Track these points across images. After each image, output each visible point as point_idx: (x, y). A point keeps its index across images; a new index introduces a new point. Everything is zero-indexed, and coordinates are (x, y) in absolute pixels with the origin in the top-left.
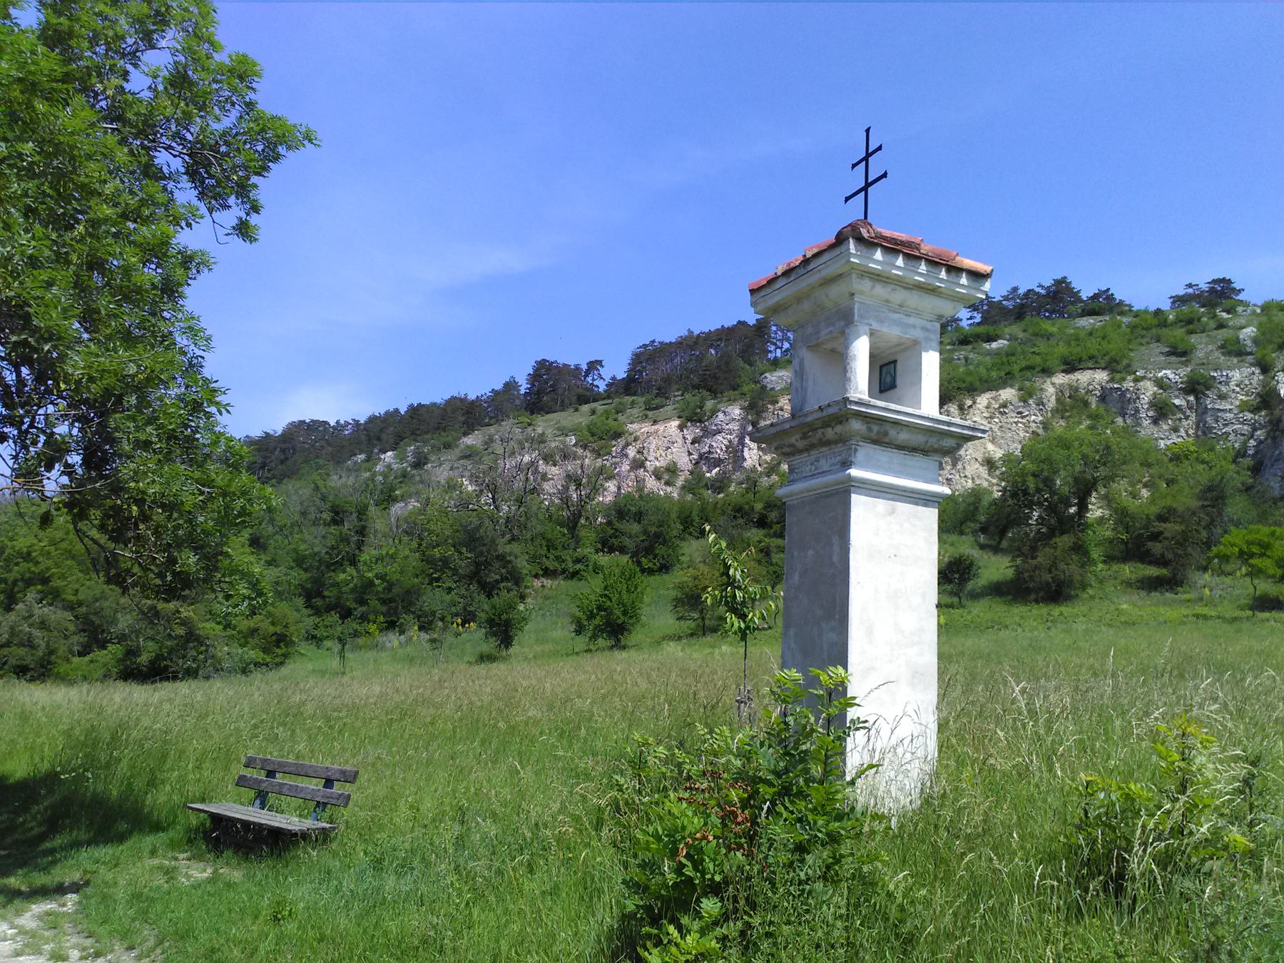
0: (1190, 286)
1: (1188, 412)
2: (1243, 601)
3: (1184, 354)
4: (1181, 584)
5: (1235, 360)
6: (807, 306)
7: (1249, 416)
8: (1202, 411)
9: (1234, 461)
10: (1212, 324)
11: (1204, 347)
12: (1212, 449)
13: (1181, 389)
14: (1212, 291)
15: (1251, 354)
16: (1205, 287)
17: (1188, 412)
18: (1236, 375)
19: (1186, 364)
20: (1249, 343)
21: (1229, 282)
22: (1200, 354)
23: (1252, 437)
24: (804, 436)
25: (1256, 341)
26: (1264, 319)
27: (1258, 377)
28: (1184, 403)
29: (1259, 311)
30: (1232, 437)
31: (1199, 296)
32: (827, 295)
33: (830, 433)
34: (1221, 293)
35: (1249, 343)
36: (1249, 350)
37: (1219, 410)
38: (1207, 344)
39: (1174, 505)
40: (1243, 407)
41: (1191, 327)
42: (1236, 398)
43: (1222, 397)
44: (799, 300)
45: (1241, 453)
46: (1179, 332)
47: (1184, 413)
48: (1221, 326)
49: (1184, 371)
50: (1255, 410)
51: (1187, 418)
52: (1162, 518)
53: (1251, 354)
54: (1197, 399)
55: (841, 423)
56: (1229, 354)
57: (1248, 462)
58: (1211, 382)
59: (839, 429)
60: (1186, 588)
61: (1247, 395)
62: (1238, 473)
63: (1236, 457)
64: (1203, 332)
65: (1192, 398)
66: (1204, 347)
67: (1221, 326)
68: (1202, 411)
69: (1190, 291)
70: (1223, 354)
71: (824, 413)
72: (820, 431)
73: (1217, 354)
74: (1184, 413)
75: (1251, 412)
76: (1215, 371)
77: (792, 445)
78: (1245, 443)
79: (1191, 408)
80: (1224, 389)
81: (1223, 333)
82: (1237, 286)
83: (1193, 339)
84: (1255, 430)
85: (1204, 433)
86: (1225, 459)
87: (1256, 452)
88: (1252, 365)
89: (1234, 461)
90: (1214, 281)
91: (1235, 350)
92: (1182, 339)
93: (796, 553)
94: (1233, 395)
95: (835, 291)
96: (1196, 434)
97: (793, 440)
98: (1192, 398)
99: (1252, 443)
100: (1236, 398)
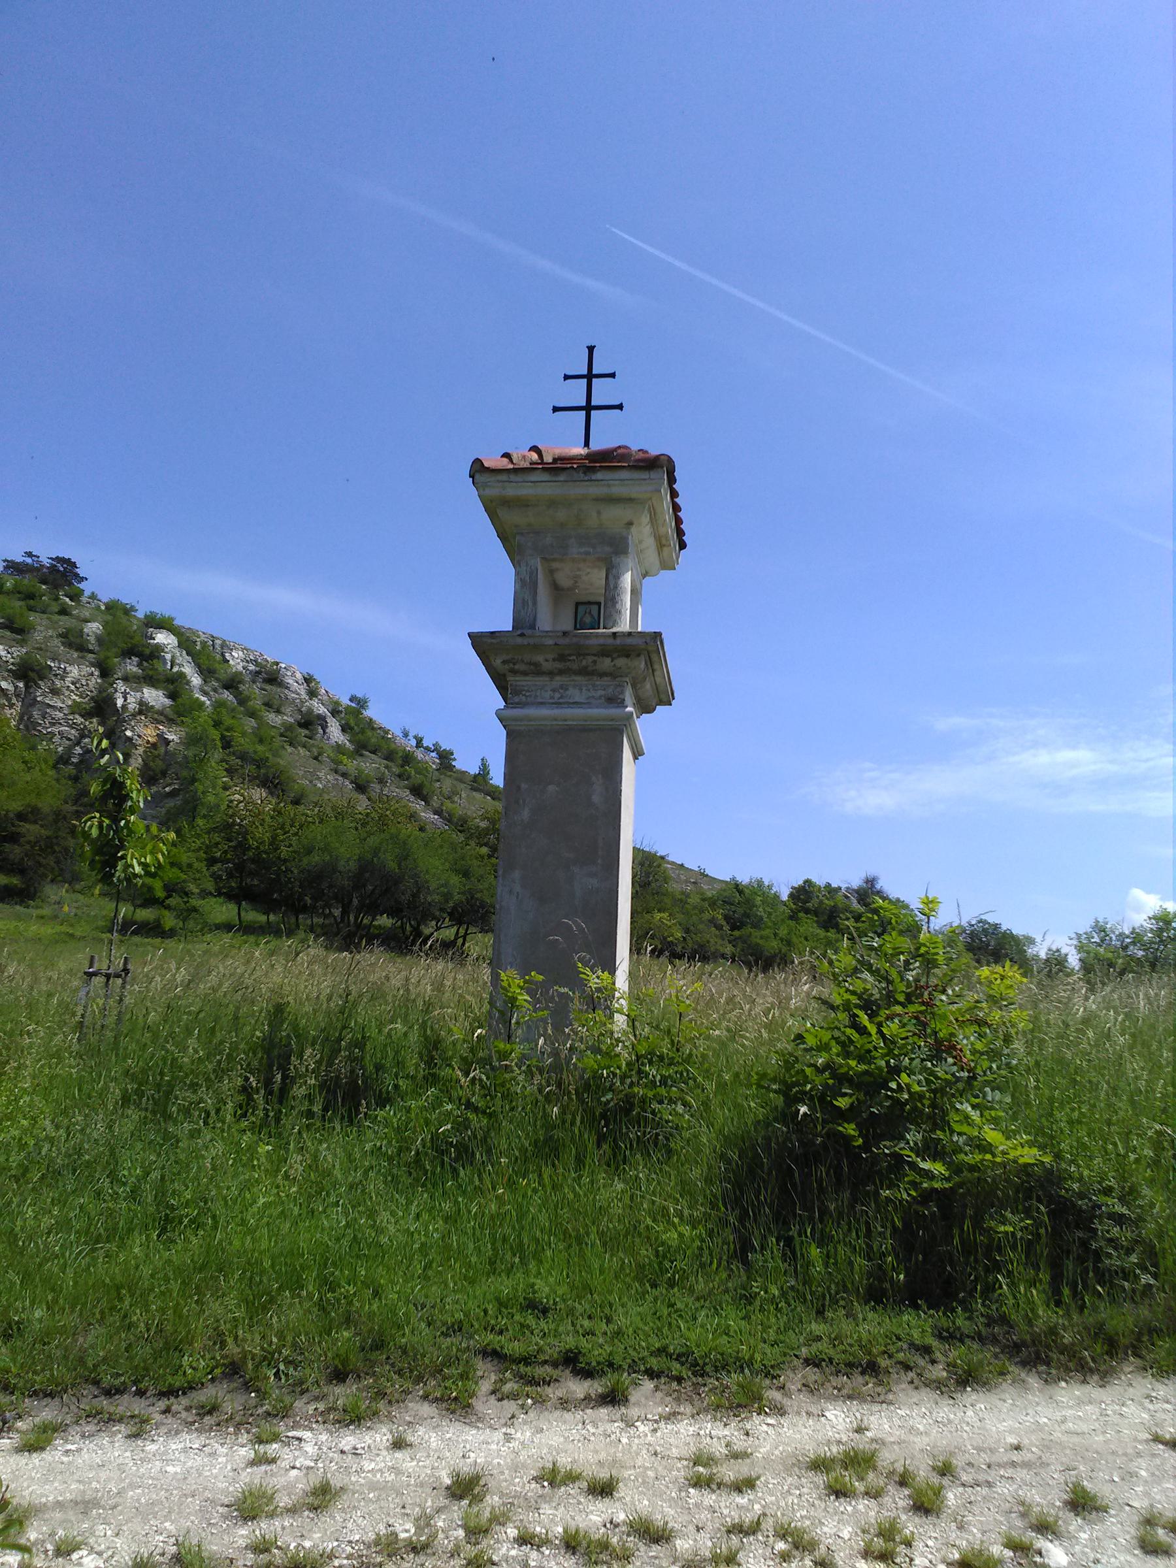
0: (29, 554)
1: (14, 701)
2: (101, 923)
3: (20, 631)
4: (32, 898)
5: (75, 655)
6: (561, 515)
7: (79, 720)
8: (30, 703)
9: (55, 767)
10: (55, 608)
11: (43, 630)
12: (33, 748)
13: (10, 671)
14: (53, 569)
15: (91, 652)
16: (46, 562)
17: (14, 701)
18: (74, 672)
19: (22, 643)
20: (92, 639)
21: (74, 565)
22: (38, 636)
23: (78, 743)
24: (562, 658)
25: (100, 640)
26: (110, 618)
27: (96, 680)
28: (11, 688)
29: (103, 608)
30: (56, 739)
31: (38, 570)
32: (599, 513)
33: (606, 664)
34: (62, 574)
35: (92, 639)
36: (91, 647)
37: (49, 706)
38: (47, 628)
39: (40, 805)
40: (75, 709)
41: (31, 602)
42: (69, 697)
43: (55, 692)
44: (552, 503)
45: (64, 759)
46: (18, 604)
47: (9, 700)
48: (64, 611)
49: (19, 652)
50: (87, 715)
51: (11, 706)
52: (21, 816)
53: (91, 652)
54: (27, 686)
55: (628, 656)
56: (70, 645)
57: (70, 770)
58: (46, 672)
59: (621, 662)
60: (38, 902)
61: (81, 697)
62: (58, 780)
63: (58, 763)
64: (44, 612)
65: (21, 685)
66: (43, 630)
67: (64, 611)
68: (30, 703)
69: (29, 560)
70: (63, 644)
71: (618, 641)
72: (590, 659)
73: (57, 642)
74: (9, 700)
75: (82, 716)
76: (53, 660)
77: (537, 665)
78: (69, 750)
79: (17, 696)
80: (58, 683)
81: (65, 622)
82: (81, 572)
83: (33, 617)
84: (83, 736)
85: (27, 727)
86: (46, 761)
87: (81, 762)
88: (92, 665)
89: (55, 767)
90: (58, 559)
91: (75, 642)
92: (22, 615)
93: (524, 786)
94: (67, 693)
95: (613, 516)
96: (17, 727)
97: (540, 658)
98: (21, 685)
99: (78, 750)
100: (69, 697)
